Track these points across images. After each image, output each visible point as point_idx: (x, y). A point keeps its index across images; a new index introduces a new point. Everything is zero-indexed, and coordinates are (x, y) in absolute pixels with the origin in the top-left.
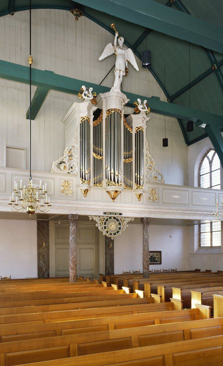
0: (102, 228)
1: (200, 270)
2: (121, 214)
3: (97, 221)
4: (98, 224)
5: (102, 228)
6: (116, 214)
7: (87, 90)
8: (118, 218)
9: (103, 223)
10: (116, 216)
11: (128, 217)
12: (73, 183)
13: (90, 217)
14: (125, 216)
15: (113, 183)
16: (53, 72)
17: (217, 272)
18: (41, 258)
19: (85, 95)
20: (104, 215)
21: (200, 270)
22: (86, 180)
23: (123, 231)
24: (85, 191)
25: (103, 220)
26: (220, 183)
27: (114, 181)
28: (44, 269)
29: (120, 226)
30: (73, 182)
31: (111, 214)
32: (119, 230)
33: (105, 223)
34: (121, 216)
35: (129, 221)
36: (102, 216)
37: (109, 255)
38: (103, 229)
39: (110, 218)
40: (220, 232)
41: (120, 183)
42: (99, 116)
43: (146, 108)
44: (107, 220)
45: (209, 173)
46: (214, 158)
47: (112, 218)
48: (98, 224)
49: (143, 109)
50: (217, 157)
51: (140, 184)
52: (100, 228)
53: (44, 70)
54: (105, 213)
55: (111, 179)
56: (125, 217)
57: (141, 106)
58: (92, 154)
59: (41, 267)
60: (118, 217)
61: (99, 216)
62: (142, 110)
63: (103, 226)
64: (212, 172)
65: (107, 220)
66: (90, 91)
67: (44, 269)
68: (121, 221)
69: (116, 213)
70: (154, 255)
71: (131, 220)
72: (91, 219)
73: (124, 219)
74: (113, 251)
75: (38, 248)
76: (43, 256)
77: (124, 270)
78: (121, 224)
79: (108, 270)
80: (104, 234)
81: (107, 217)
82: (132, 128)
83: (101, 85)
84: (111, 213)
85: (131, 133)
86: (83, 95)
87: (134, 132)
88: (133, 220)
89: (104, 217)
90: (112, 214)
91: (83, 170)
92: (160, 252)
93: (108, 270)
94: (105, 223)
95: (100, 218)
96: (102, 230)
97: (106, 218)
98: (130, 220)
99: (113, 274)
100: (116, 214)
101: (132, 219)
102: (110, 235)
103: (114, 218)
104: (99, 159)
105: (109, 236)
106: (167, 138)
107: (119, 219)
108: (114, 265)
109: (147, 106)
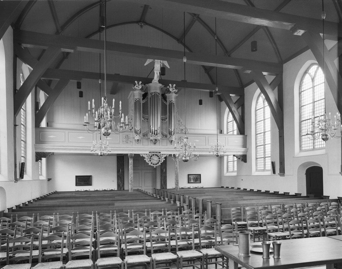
1: (329, 196)
2: (160, 153)
6: (157, 152)
7: (138, 83)
8: (158, 155)
13: (141, 155)
14: (162, 154)
15: (154, 135)
17: (337, 198)
18: (119, 179)
19: (137, 87)
21: (329, 196)
22: (138, 134)
23: (161, 162)
24: (137, 140)
26: (270, 117)
27: (155, 134)
28: (121, 185)
29: (159, 160)
33: (150, 158)
39: (153, 155)
40: (236, 161)
41: (158, 135)
42: (146, 97)
43: (175, 89)
44: (151, 156)
45: (312, 88)
46: (317, 74)
49: (172, 90)
50: (320, 71)
51: (171, 135)
52: (147, 161)
53: (114, 74)
54: (150, 152)
55: (153, 133)
56: (163, 154)
57: (172, 89)
61: (147, 154)
62: (172, 91)
64: (315, 86)
65: (151, 156)
66: (140, 83)
67: (121, 185)
76: (121, 178)
80: (149, 164)
82: (167, 101)
83: (148, 77)
84: (153, 152)
86: (135, 87)
87: (168, 104)
91: (137, 129)
92: (200, 175)
95: (147, 155)
96: (148, 162)
97: (151, 155)
99: (166, 189)
107: (158, 155)
108: (166, 183)
109: (175, 88)
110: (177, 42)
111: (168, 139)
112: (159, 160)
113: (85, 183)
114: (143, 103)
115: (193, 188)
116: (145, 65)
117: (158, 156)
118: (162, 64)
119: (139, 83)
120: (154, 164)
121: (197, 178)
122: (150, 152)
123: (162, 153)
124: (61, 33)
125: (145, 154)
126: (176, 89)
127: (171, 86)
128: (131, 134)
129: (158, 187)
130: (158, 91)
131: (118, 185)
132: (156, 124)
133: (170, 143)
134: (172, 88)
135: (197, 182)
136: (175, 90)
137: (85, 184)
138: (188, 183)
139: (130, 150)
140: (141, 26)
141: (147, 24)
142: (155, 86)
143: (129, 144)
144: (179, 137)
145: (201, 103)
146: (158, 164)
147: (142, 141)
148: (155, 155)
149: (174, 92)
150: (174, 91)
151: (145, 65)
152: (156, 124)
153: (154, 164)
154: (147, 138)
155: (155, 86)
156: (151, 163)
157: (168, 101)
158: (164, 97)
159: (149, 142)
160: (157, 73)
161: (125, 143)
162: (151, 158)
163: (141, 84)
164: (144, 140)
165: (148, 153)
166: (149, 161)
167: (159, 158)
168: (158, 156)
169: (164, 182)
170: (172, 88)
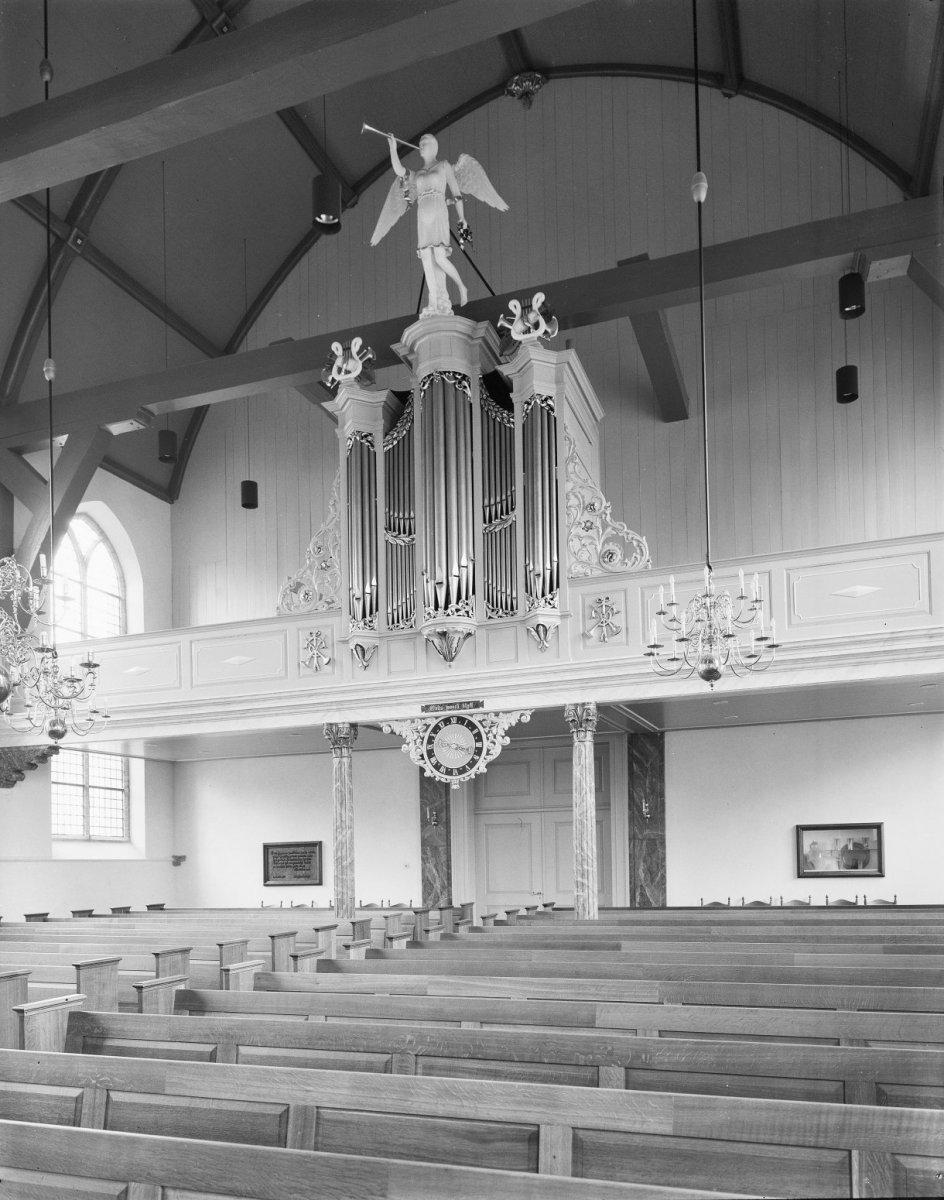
0: (422, 756)
2: (477, 705)
3: (404, 736)
4: (408, 744)
5: (422, 756)
6: (461, 705)
9: (423, 739)
10: (462, 711)
11: (509, 712)
12: (333, 635)
16: (643, 258)
20: (424, 714)
23: (490, 758)
25: (425, 731)
28: (438, 885)
29: (479, 745)
30: (333, 631)
31: (445, 710)
32: (476, 757)
33: (431, 740)
34: (481, 709)
35: (514, 724)
36: (421, 719)
37: (644, 843)
38: (423, 758)
39: (447, 721)
44: (436, 729)
47: (454, 720)
48: (408, 744)
49: (528, 331)
53: (614, 266)
54: (426, 709)
56: (497, 714)
58: (383, 535)
59: (430, 878)
60: (471, 715)
62: (527, 336)
63: (424, 750)
65: (436, 729)
67: (438, 885)
68: (484, 727)
69: (461, 703)
70: (866, 840)
71: (519, 720)
72: (386, 730)
73: (495, 719)
74: (663, 830)
75: (422, 826)
76: (435, 849)
77: (704, 897)
78: (484, 736)
79: (642, 895)
81: (437, 718)
84: (444, 706)
85: (510, 428)
88: (526, 719)
89: (428, 722)
90: (448, 707)
93: (642, 895)
94: (431, 740)
98: (513, 720)
100: (461, 708)
101: (521, 716)
102: (446, 777)
103: (461, 720)
104: (403, 544)
105: (443, 780)
106: (856, 365)
107: (475, 720)
108: (663, 877)
110: (719, 92)
111: (523, 622)
112: (479, 745)
113: (298, 873)
114: (387, 454)
115: (827, 908)
116: (375, 240)
117: (471, 726)
118: (460, 205)
119: (350, 348)
120: (449, 772)
121: (864, 851)
122: (426, 709)
123: (489, 706)
124: (71, 240)
125: (404, 720)
126: (548, 320)
127: (517, 311)
128: (334, 621)
129: (621, 897)
130: (460, 366)
131: (427, 885)
132: (455, 554)
133: (533, 644)
134: (527, 328)
135: (860, 870)
136: (543, 326)
137: (299, 877)
138: (799, 876)
139: (340, 705)
140: (526, 96)
141: (548, 72)
142: (439, 341)
143: (326, 674)
144: (590, 601)
145: (847, 387)
146: (474, 769)
147: (382, 651)
148: (454, 720)
149: (539, 338)
150: (540, 332)
151: (375, 240)
152: (455, 554)
153: (449, 772)
154: (410, 631)
155: (439, 341)
156: (437, 767)
157: (517, 408)
158: (498, 389)
159: (422, 656)
160: (436, 265)
161: (309, 671)
162: (438, 737)
163: (358, 353)
164: (397, 647)
165: (417, 712)
166: (426, 756)
167: (478, 737)
168: (471, 726)
169: (650, 872)
170: (527, 328)
